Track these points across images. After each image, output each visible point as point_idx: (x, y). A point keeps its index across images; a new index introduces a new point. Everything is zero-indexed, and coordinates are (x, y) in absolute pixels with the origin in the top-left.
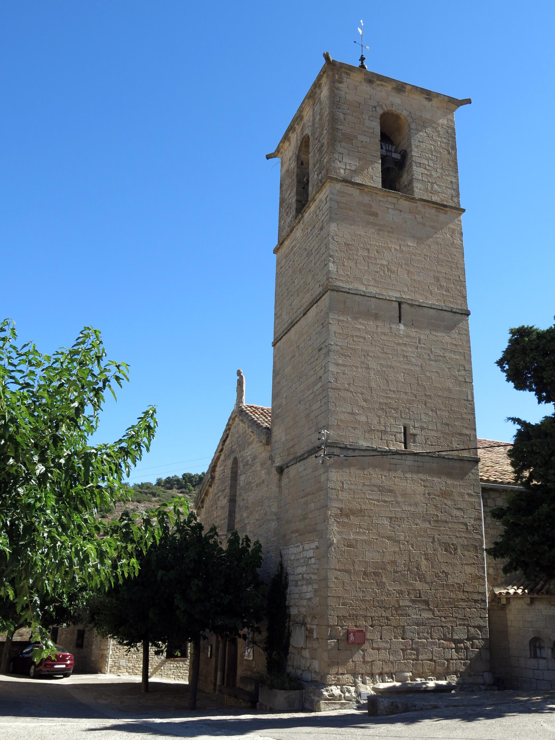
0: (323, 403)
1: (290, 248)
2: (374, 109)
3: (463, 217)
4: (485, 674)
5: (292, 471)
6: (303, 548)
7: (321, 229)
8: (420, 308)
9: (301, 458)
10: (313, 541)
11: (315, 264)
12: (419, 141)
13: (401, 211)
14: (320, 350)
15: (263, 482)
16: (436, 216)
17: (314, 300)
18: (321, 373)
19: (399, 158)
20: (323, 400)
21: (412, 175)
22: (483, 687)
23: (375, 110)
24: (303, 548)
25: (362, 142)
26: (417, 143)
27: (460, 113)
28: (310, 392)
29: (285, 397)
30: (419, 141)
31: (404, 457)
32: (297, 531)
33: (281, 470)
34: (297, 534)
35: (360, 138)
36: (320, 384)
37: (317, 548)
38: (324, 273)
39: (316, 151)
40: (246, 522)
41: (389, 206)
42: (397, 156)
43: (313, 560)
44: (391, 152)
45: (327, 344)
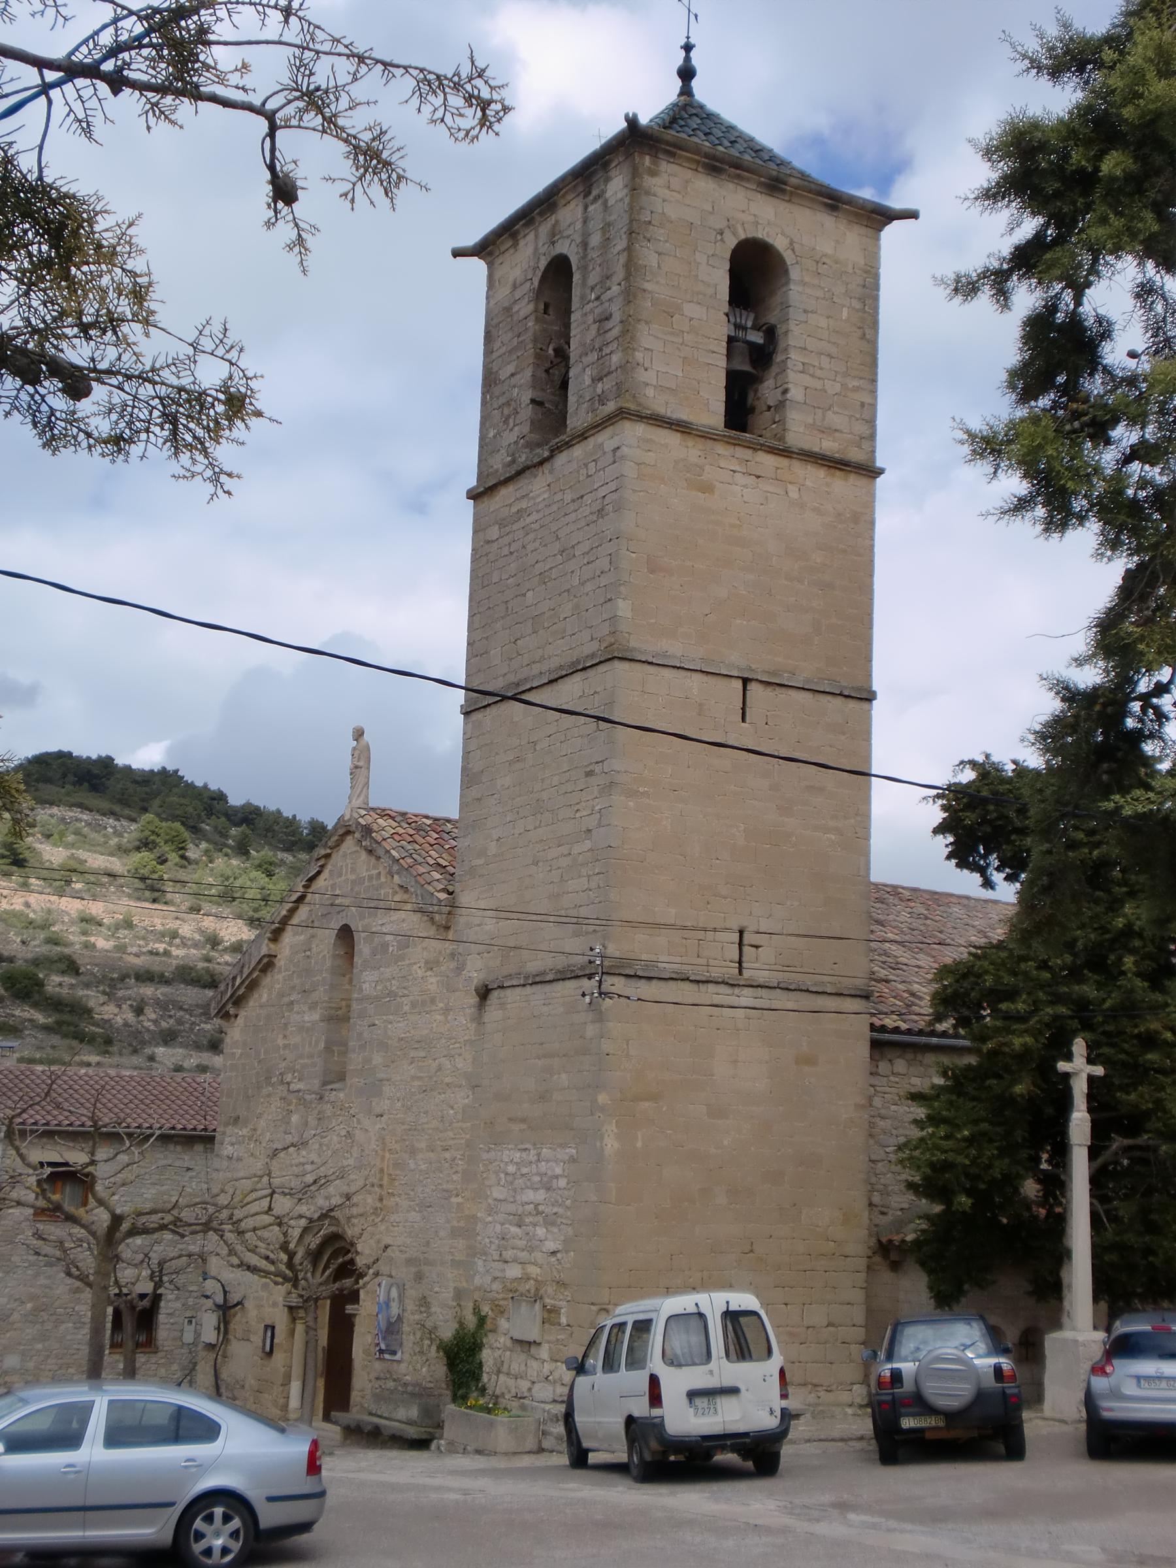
0: (593, 885)
1: (514, 509)
2: (719, 237)
3: (880, 480)
4: (855, 1387)
5: (511, 1003)
6: (539, 1154)
7: (601, 512)
8: (783, 690)
9: (538, 979)
10: (563, 1146)
11: (583, 584)
12: (805, 311)
13: (758, 477)
14: (589, 774)
15: (433, 1001)
16: (828, 485)
17: (578, 662)
18: (592, 822)
19: (761, 341)
20: (596, 878)
21: (786, 391)
22: (849, 1411)
23: (722, 240)
24: (539, 1154)
25: (691, 319)
26: (803, 317)
27: (892, 233)
28: (564, 849)
29: (495, 837)
30: (805, 311)
31: (737, 991)
32: (523, 1120)
33: (484, 993)
34: (523, 1126)
35: (691, 310)
36: (588, 844)
37: (573, 1160)
38: (605, 616)
39: (590, 318)
40: (381, 1075)
41: (737, 468)
42: (757, 338)
43: (562, 1183)
44: (745, 329)
45: (606, 767)
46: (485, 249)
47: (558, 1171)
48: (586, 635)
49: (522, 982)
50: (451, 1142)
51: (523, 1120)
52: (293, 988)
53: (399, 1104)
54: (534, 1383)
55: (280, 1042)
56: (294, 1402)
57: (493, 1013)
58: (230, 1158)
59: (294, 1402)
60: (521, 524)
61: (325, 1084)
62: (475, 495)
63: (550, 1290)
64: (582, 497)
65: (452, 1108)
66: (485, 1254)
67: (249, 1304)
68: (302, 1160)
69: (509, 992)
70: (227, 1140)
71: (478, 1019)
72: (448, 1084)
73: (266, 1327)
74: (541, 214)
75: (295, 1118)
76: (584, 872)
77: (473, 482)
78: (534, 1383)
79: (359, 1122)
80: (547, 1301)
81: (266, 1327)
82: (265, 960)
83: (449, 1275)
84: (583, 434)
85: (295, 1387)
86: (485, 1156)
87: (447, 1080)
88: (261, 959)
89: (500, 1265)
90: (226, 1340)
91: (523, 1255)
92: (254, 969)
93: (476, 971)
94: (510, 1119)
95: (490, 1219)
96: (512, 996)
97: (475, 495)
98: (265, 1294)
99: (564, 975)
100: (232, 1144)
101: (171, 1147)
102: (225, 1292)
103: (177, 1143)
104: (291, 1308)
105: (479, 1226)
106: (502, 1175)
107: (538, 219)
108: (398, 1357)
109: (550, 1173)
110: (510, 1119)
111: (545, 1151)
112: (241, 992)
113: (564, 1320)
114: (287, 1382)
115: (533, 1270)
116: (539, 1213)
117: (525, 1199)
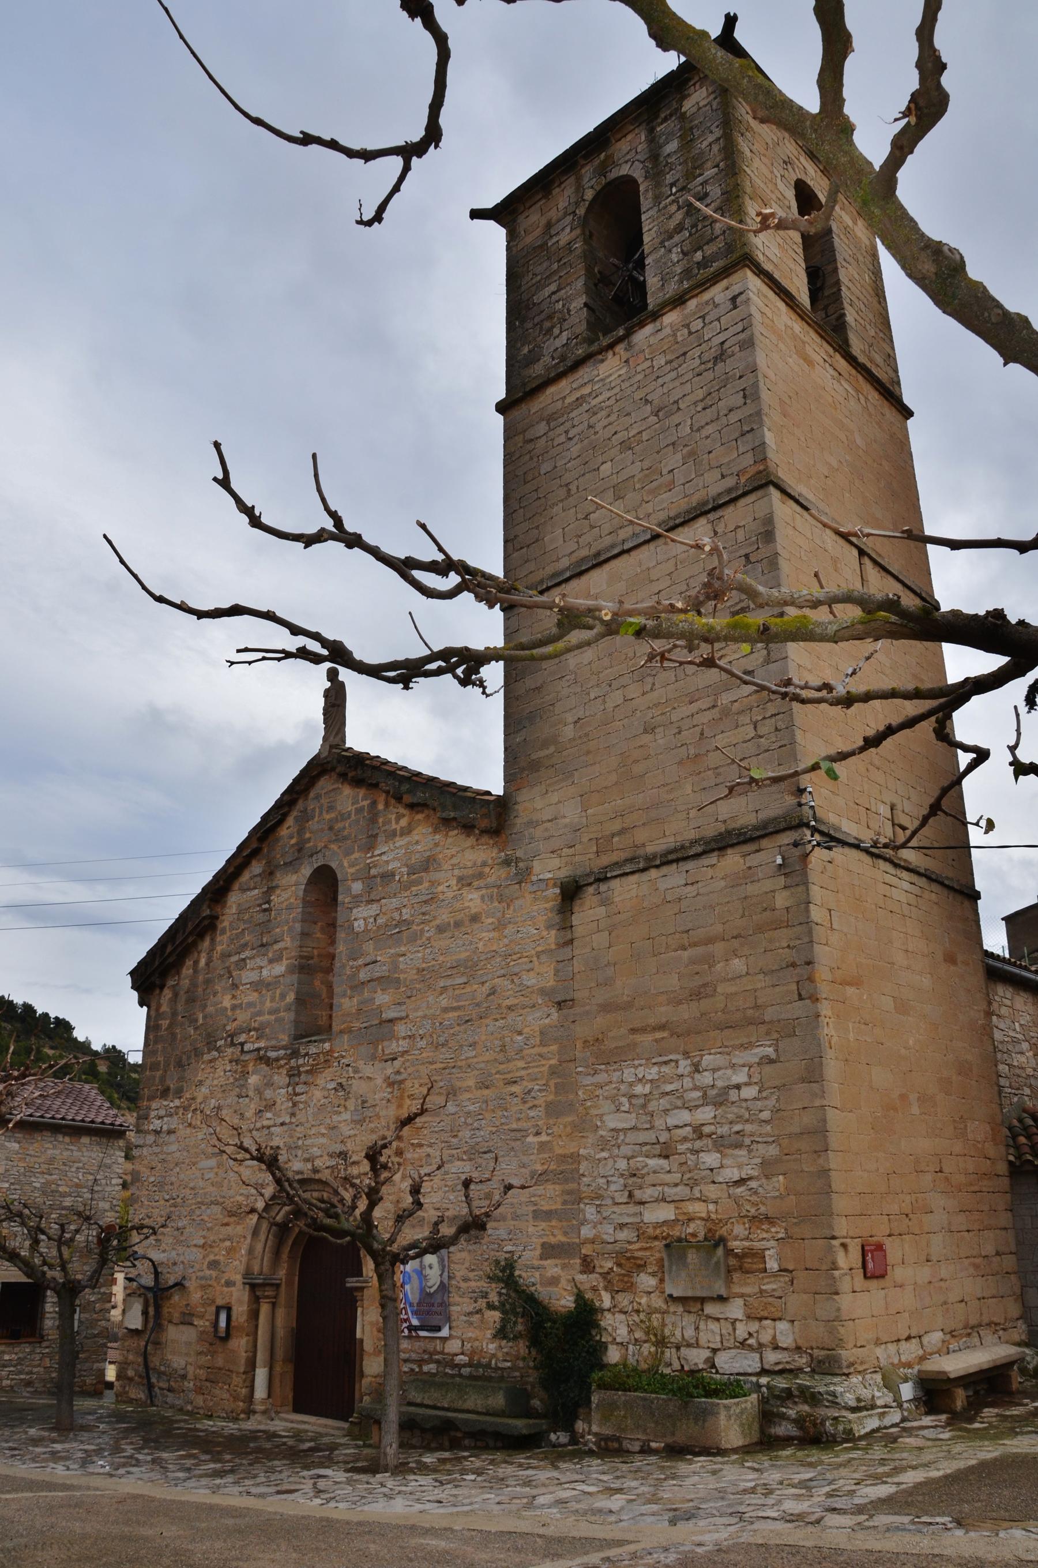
32: (662, 1027)
46: (504, 213)
47: (740, 1077)
48: (713, 476)
49: (641, 866)
50: (523, 1073)
51: (662, 1027)
52: (246, 945)
53: (423, 1043)
54: (715, 1351)
55: (227, 1002)
56: (260, 1392)
57: (588, 912)
58: (157, 1132)
59: (260, 1392)
60: (585, 407)
61: (297, 1037)
62: (502, 408)
63: (739, 1230)
64: (685, 354)
65: (520, 1033)
66: (600, 1197)
67: (191, 1285)
68: (266, 1123)
69: (615, 884)
70: (153, 1114)
71: (565, 926)
72: (509, 1008)
73: (218, 1309)
74: (585, 157)
75: (253, 1080)
76: (745, 719)
77: (502, 394)
78: (715, 1351)
79: (356, 1071)
80: (734, 1244)
81: (218, 1309)
82: (206, 922)
83: (531, 1229)
84: (681, 297)
85: (261, 1375)
86: (588, 1080)
87: (508, 1002)
88: (200, 922)
89: (632, 1209)
90: (158, 1327)
91: (682, 1191)
92: (190, 933)
93: (550, 868)
94: (633, 1031)
95: (605, 1154)
96: (625, 891)
97: (502, 408)
98: (214, 1273)
99: (721, 843)
100: (160, 1118)
101: (60, 1138)
102: (157, 1274)
103: (65, 1134)
104: (253, 1287)
105: (583, 1167)
106: (624, 1100)
107: (583, 162)
108: (445, 1332)
109: (720, 1084)
110: (633, 1031)
111: (707, 1060)
112: (171, 960)
113: (772, 1265)
114: (252, 1365)
115: (698, 1209)
116: (701, 1136)
117: (671, 1121)
